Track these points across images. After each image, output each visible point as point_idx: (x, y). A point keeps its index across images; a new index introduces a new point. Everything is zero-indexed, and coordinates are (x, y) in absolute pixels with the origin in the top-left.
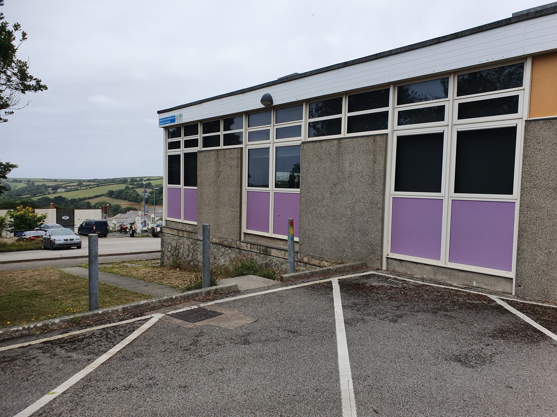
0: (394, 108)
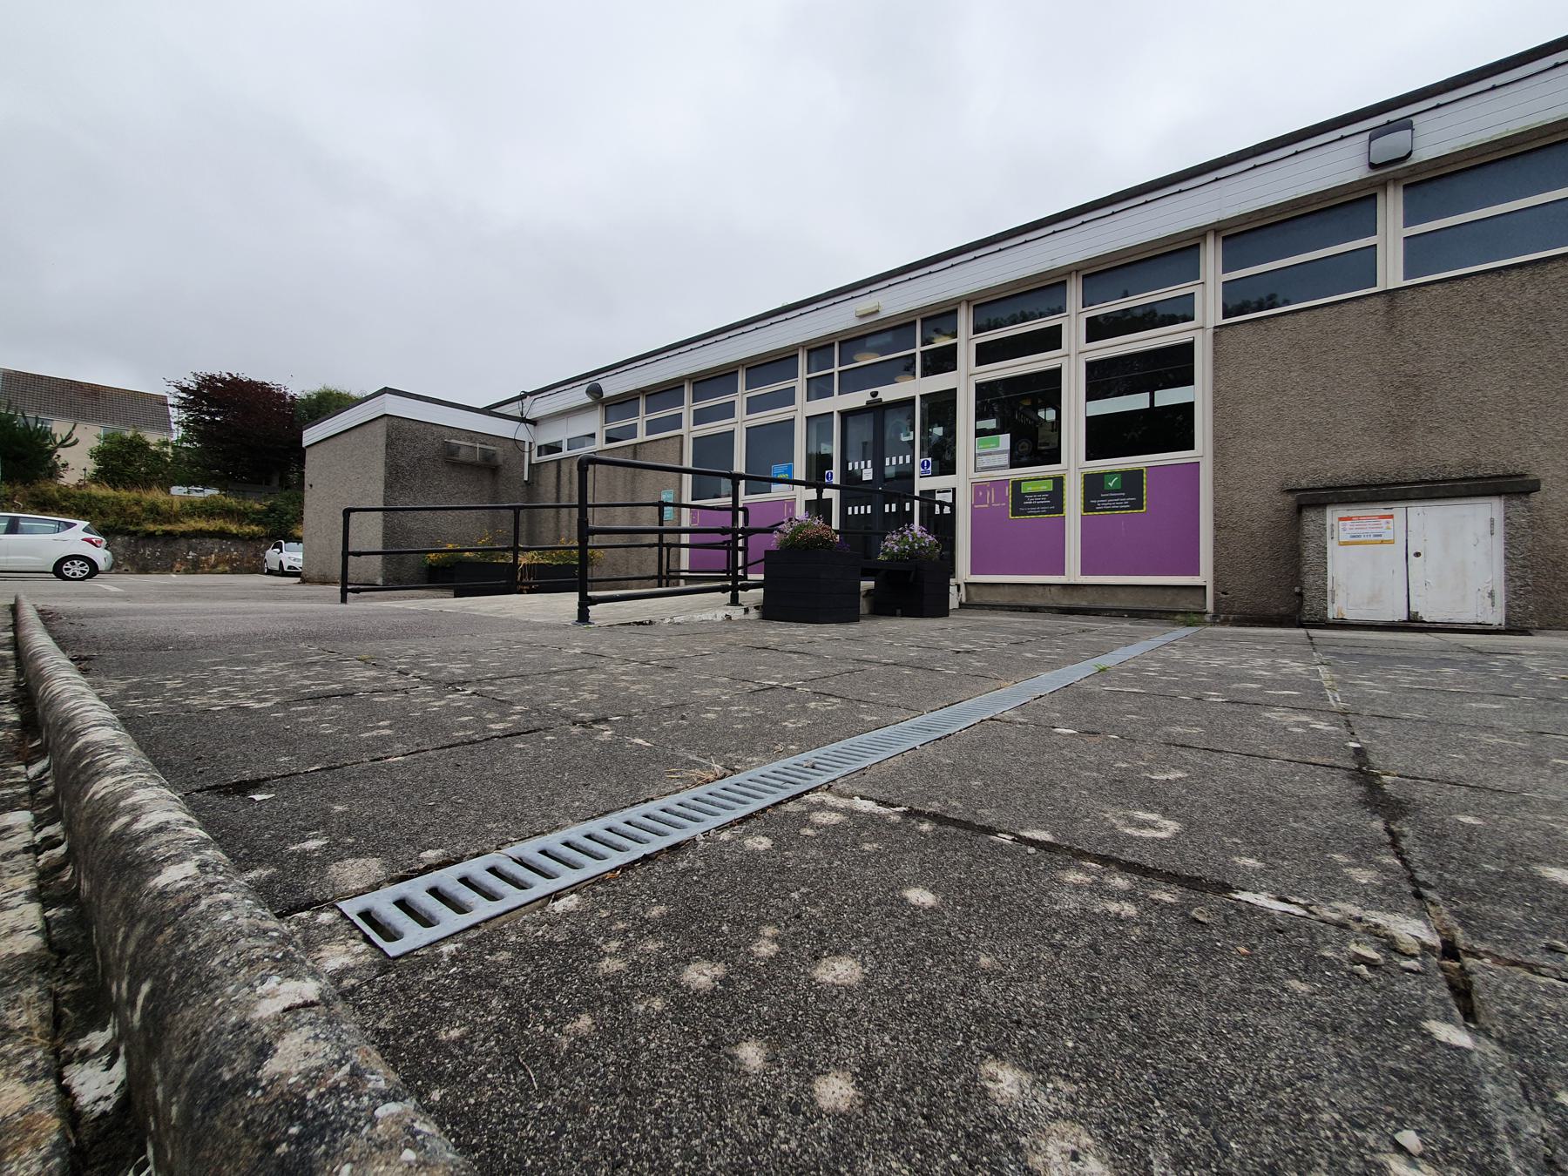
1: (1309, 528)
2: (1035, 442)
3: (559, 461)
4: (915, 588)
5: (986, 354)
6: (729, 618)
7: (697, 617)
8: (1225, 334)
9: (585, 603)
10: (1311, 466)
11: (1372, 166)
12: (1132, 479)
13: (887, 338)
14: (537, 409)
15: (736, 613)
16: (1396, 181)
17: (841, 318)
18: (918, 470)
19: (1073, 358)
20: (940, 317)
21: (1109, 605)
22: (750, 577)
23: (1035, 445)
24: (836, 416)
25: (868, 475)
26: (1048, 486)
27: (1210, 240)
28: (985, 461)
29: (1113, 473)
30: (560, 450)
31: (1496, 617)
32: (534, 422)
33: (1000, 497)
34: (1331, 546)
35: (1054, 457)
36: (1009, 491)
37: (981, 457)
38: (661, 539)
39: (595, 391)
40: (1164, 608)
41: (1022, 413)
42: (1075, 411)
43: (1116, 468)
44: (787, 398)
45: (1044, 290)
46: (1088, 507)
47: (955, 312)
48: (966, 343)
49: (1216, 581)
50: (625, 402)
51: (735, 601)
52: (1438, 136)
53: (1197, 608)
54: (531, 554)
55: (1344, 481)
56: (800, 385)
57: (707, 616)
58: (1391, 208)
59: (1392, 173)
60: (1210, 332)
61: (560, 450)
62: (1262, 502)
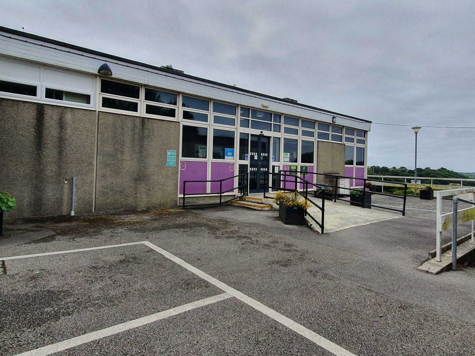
17: (256, 103)
26: (295, 168)
38: (296, 180)
39: (104, 70)
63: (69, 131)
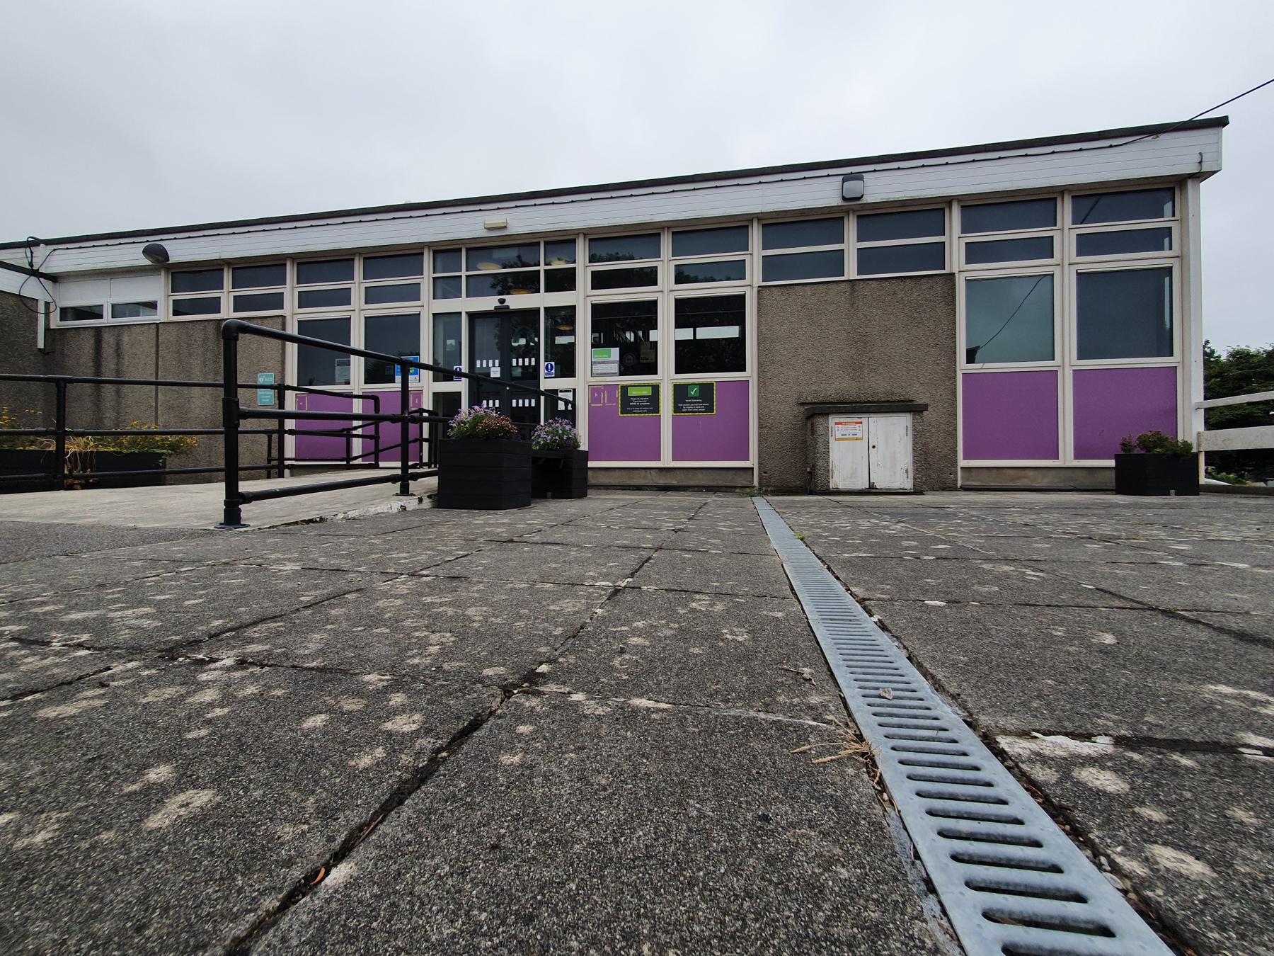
0: (293, 288)
1: (820, 429)
2: (638, 357)
3: (98, 331)
4: (560, 474)
5: (600, 281)
6: (404, 508)
7: (373, 510)
8: (766, 293)
9: (235, 500)
10: (814, 388)
11: (844, 199)
12: (706, 389)
13: (512, 254)
14: (62, 261)
15: (411, 503)
16: (854, 211)
17: (471, 226)
18: (542, 371)
19: (666, 294)
20: (562, 242)
21: (691, 483)
22: (381, 464)
23: (639, 360)
24: (464, 315)
25: (496, 372)
26: (647, 392)
27: (755, 224)
28: (599, 368)
29: (694, 384)
30: (101, 317)
31: (908, 485)
32: (54, 278)
33: (612, 398)
34: (831, 440)
35: (652, 369)
36: (618, 394)
37: (595, 368)
38: (282, 424)
39: (158, 256)
40: (728, 484)
41: (624, 329)
42: (666, 335)
43: (696, 381)
44: (413, 293)
45: (646, 236)
46: (677, 409)
47: (574, 241)
48: (584, 271)
49: (760, 464)
50: (205, 273)
51: (405, 491)
52: (880, 188)
53: (745, 483)
54: (82, 440)
55: (830, 399)
56: (426, 282)
57: (383, 508)
58: (851, 228)
59: (852, 205)
60: (755, 290)
61: (101, 317)
62: (787, 412)
63: (126, 361)
